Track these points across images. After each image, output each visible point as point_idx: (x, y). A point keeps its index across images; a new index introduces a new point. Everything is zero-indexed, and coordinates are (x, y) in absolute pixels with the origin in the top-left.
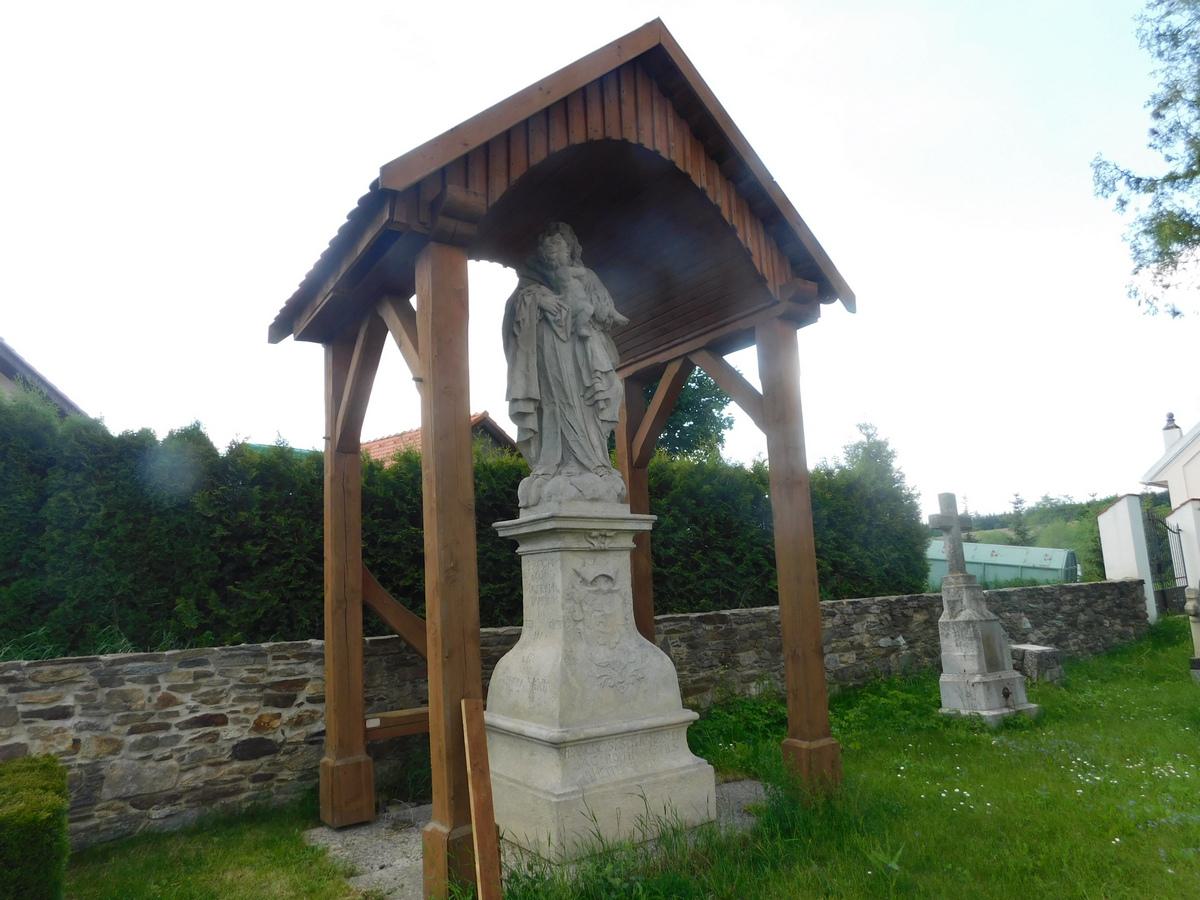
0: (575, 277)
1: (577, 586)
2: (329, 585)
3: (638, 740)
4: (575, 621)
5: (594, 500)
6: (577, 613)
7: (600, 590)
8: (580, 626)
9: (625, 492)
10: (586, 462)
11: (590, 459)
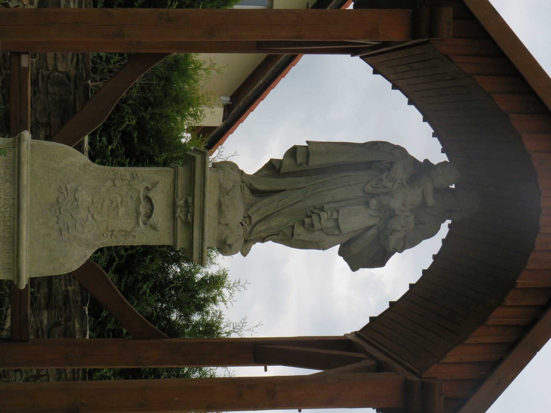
0: (423, 193)
1: (144, 183)
2: (216, 130)
3: (9, 223)
4: (114, 180)
5: (220, 205)
6: (121, 181)
7: (140, 202)
8: (109, 183)
9: (263, 367)
10: (254, 208)
11: (257, 211)
